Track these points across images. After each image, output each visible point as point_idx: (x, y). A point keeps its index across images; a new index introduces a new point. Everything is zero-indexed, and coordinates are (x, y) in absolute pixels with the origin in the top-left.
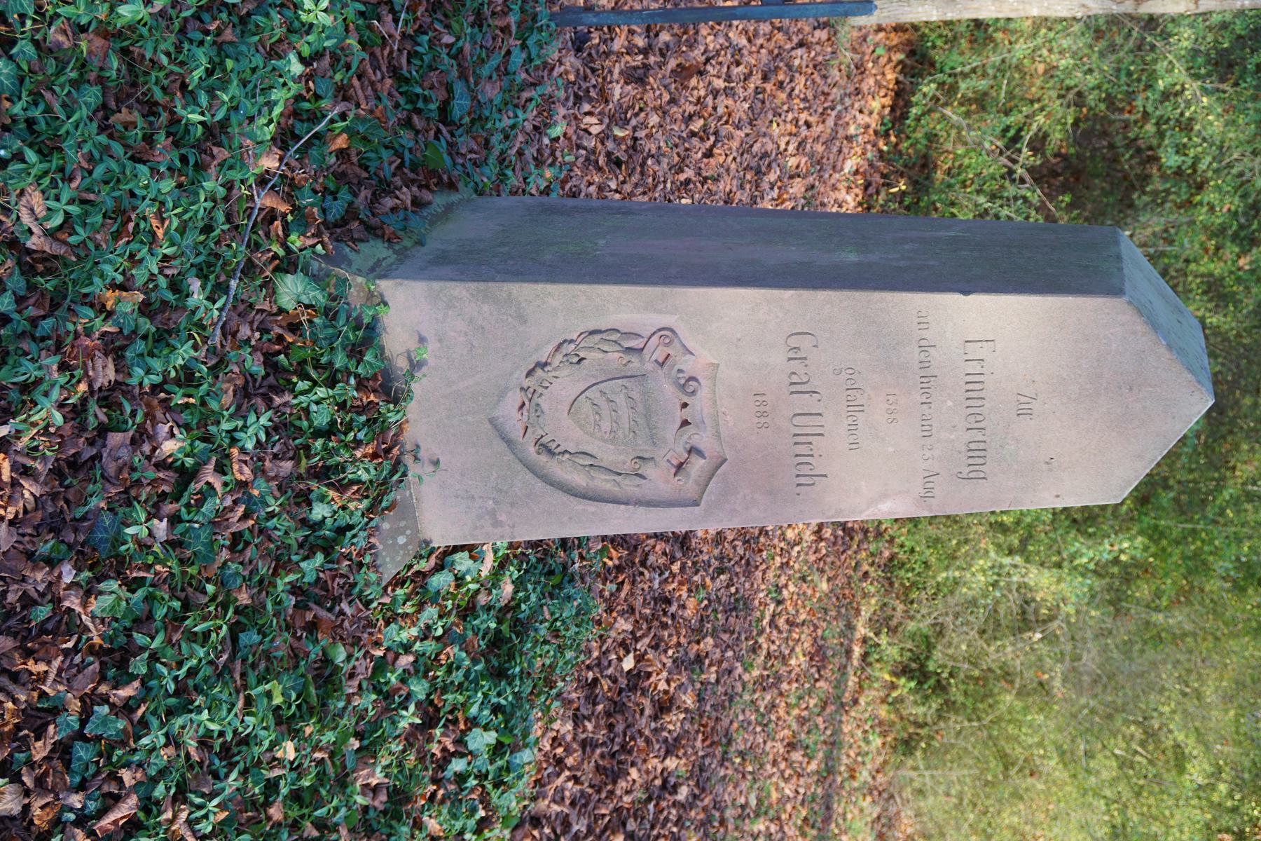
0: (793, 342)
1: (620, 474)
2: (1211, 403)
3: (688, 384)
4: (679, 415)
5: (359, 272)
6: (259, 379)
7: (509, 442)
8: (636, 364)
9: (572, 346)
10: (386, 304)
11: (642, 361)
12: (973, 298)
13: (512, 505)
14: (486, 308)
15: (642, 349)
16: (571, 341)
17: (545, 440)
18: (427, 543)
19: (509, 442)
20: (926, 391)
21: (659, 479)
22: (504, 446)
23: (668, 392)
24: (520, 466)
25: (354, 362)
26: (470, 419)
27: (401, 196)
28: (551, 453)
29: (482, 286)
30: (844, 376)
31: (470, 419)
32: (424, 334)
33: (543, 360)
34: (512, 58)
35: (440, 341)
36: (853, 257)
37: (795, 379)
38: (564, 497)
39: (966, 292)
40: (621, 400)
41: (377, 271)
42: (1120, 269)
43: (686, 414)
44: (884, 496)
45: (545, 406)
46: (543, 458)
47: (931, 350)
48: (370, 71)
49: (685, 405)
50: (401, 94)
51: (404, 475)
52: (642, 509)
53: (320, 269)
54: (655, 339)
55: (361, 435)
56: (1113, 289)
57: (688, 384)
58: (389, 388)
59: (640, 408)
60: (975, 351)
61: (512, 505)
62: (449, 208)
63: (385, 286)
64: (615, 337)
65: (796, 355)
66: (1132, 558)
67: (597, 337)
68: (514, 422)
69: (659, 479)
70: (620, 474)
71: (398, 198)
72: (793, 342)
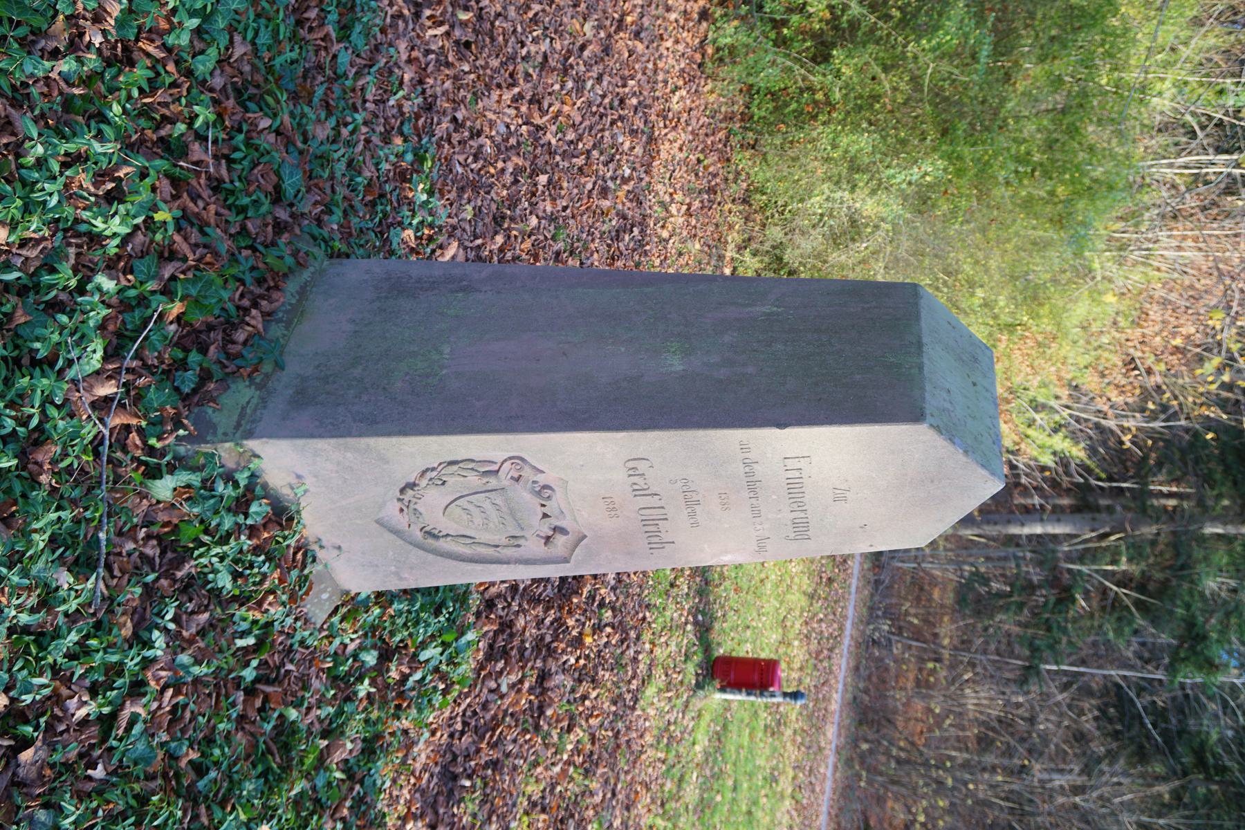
0: (631, 464)
1: (497, 546)
2: (1002, 487)
3: (543, 491)
4: (540, 511)
5: (226, 438)
6: (157, 560)
7: (397, 532)
8: (493, 482)
9: (434, 473)
10: (258, 457)
11: (499, 480)
12: (788, 431)
13: (411, 568)
14: (349, 455)
15: (498, 471)
16: (433, 469)
17: (427, 529)
18: (347, 593)
19: (397, 532)
20: (752, 490)
21: (533, 547)
22: (393, 537)
23: (524, 496)
24: (411, 547)
25: (242, 517)
26: (359, 522)
27: (253, 322)
28: (436, 537)
29: (341, 441)
30: (679, 484)
31: (359, 522)
32: (300, 473)
33: (412, 480)
34: (339, 61)
35: (316, 476)
36: (676, 364)
37: (636, 487)
38: (455, 563)
39: (781, 425)
40: (487, 505)
41: (245, 428)
42: (921, 367)
43: (545, 510)
44: (726, 552)
45: (421, 509)
46: (430, 541)
47: (755, 466)
48: (191, 205)
49: (543, 505)
50: (229, 208)
51: (310, 588)
52: (521, 567)
53: (188, 450)
54: (507, 465)
55: (265, 569)
56: (915, 415)
57: (543, 491)
58: (283, 516)
59: (504, 509)
60: (791, 464)
61: (411, 568)
62: (303, 292)
63: (252, 444)
64: (471, 465)
65: (633, 472)
66: (936, 178)
67: (455, 468)
68: (401, 521)
69: (533, 547)
70: (497, 546)
71: (248, 324)
72: (631, 464)
